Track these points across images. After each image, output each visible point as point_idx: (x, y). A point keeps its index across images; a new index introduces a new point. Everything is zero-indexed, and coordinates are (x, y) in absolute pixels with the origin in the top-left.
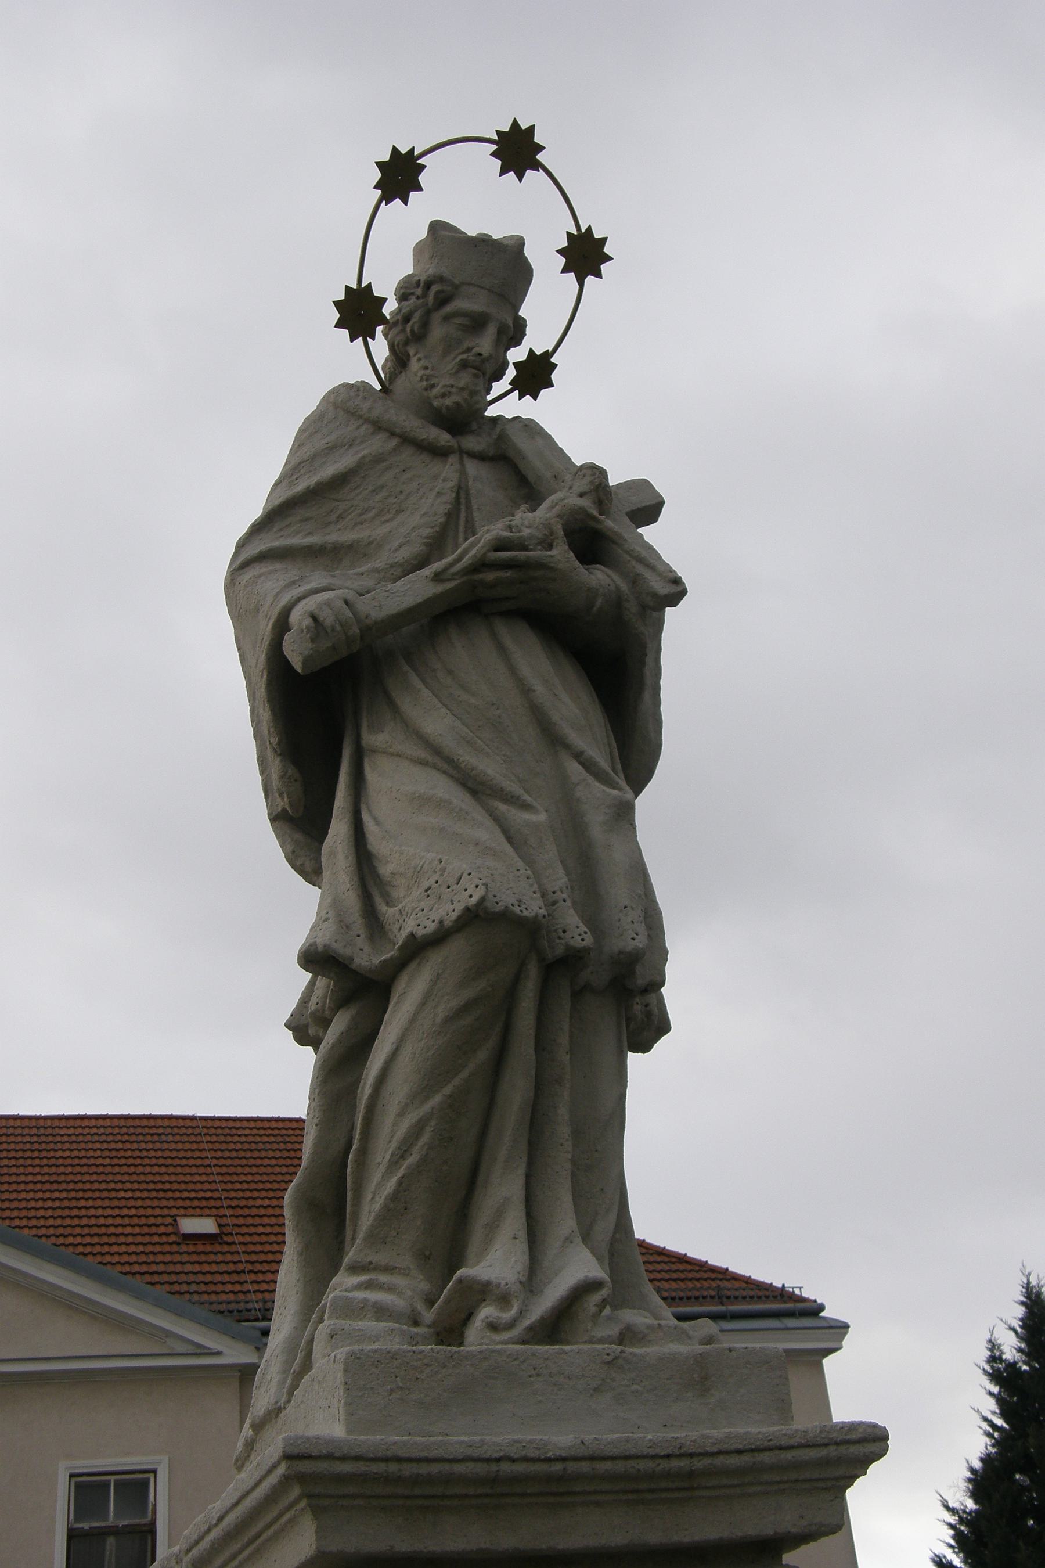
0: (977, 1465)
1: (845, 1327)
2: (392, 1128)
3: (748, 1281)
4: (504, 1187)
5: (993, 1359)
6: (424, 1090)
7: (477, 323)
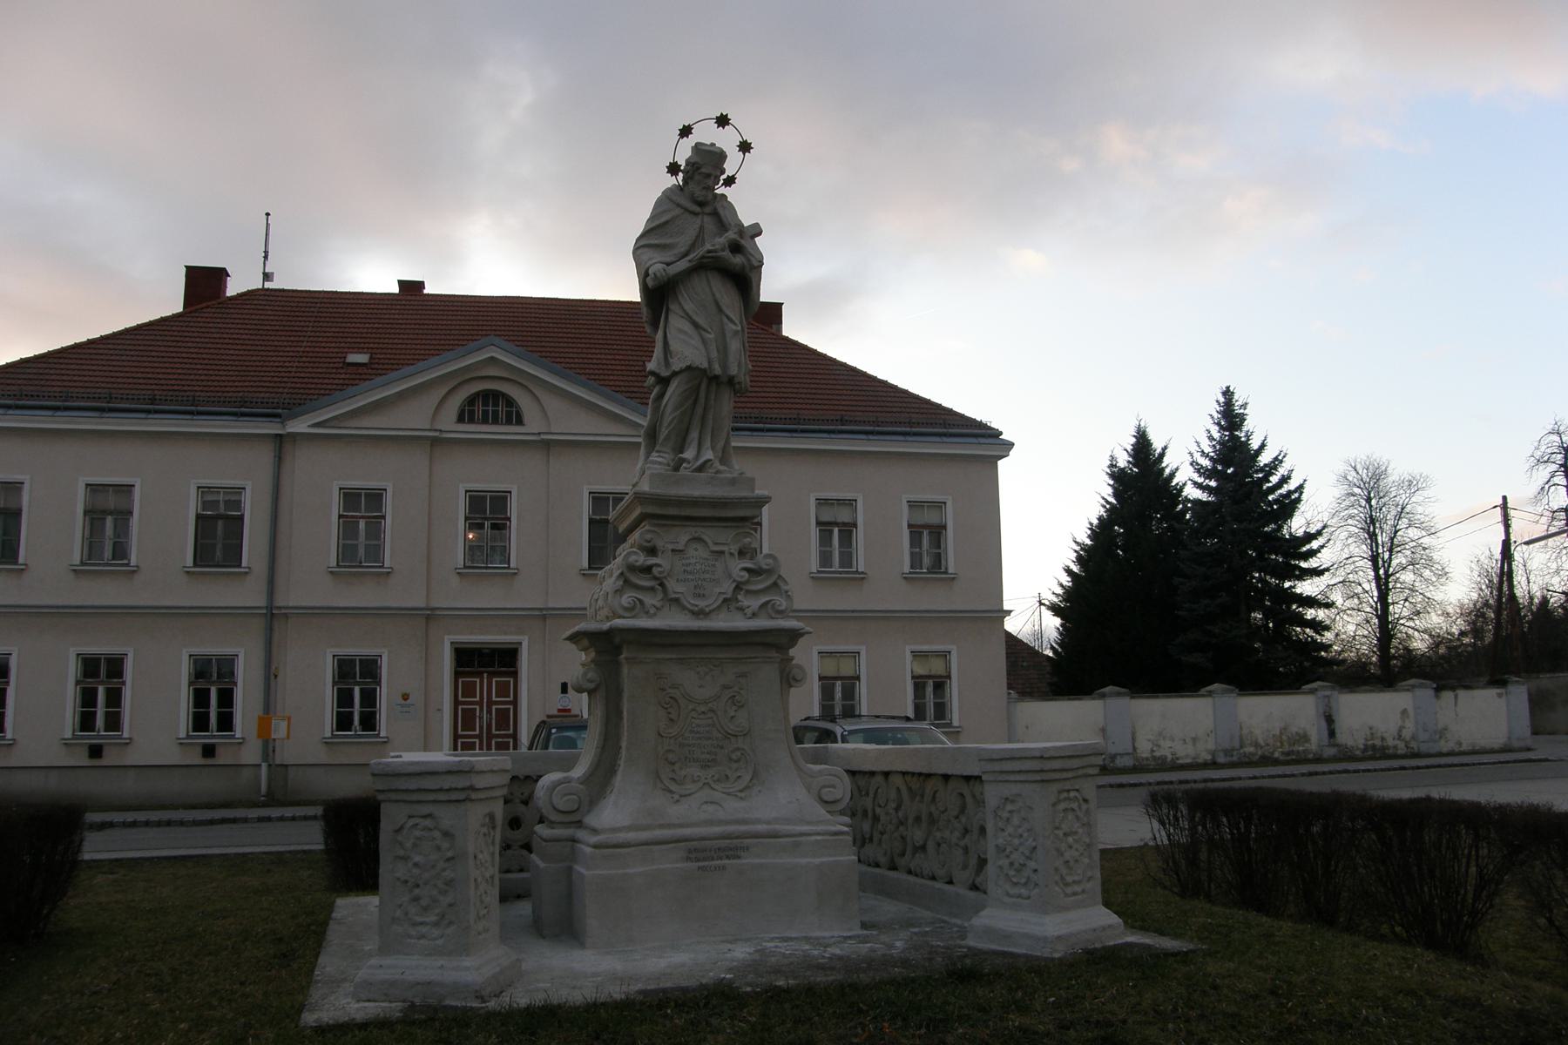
0: (1095, 522)
1: (1012, 445)
2: (668, 418)
3: (962, 416)
4: (694, 434)
5: (1112, 466)
6: (676, 409)
7: (708, 176)
